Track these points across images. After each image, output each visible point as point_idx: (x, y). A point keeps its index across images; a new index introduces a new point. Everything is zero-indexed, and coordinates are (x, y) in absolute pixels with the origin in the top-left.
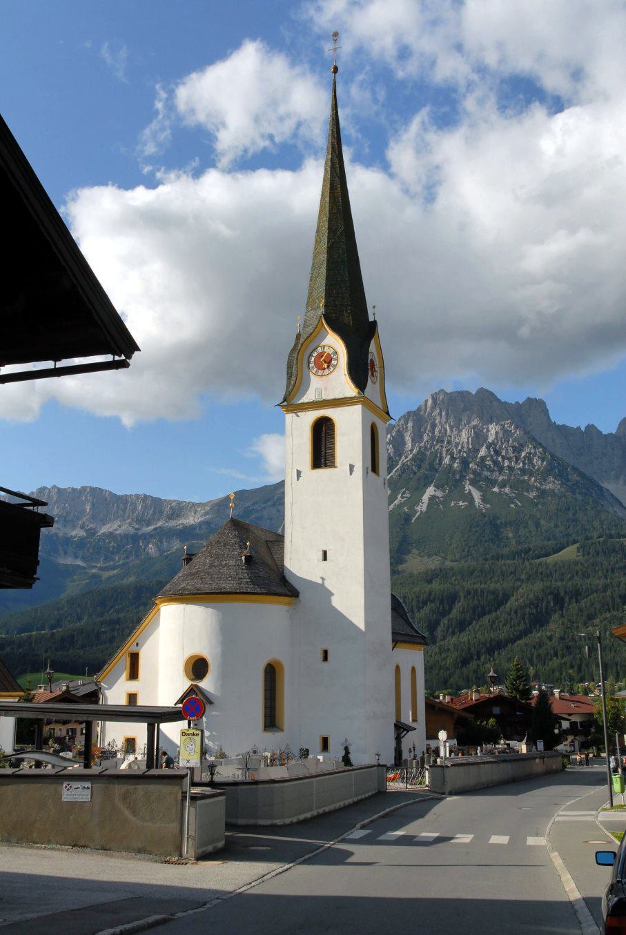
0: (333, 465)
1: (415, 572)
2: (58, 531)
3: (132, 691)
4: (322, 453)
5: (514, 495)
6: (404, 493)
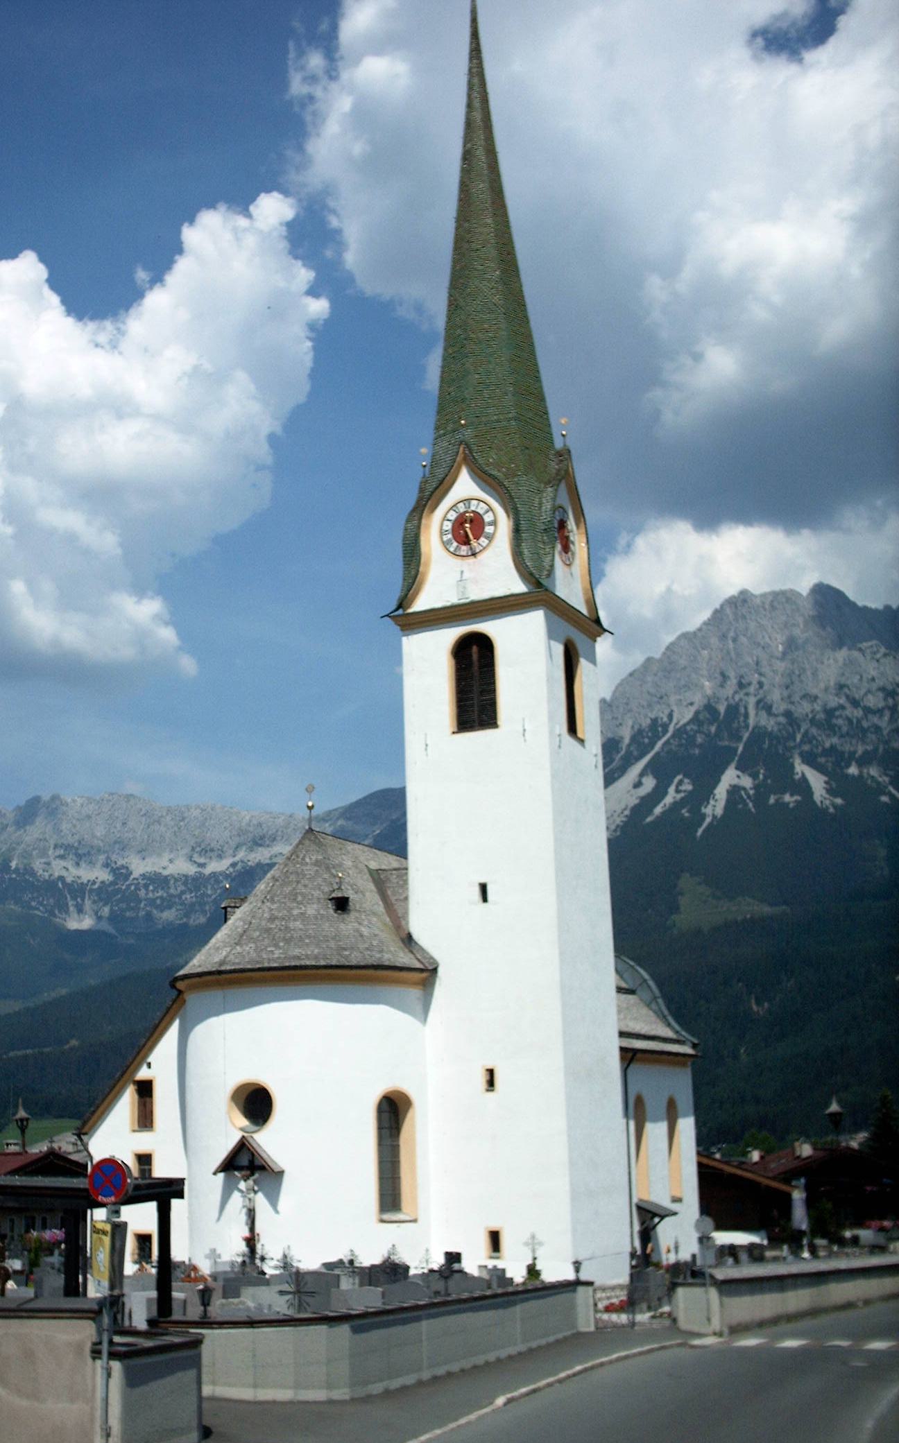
2: (64, 873)
3: (143, 1149)
4: (475, 703)
6: (680, 782)
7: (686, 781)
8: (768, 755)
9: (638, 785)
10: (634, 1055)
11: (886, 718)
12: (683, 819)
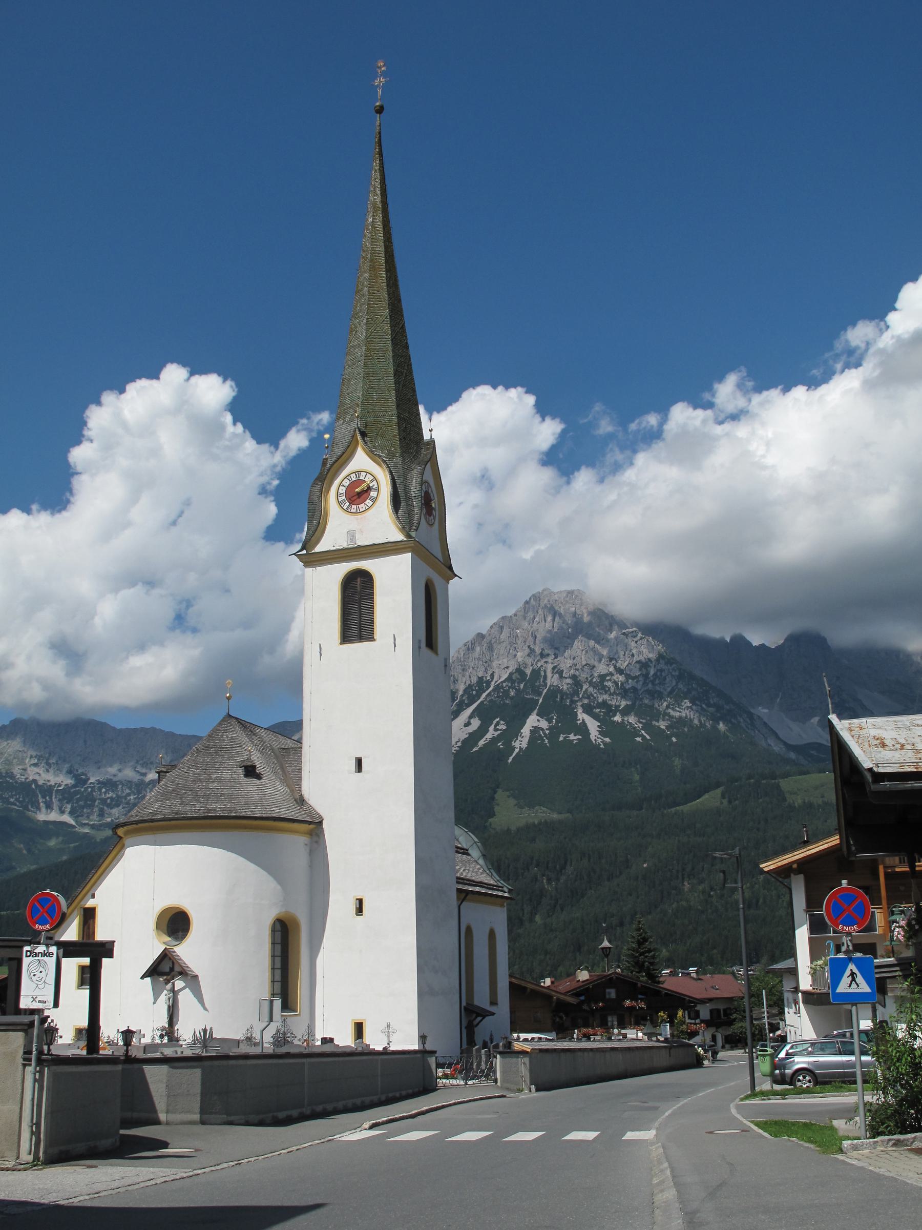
0: (372, 639)
1: (513, 828)
2: (37, 777)
4: (356, 620)
5: (640, 725)
6: (498, 723)
7: (502, 722)
8: (559, 706)
9: (467, 724)
10: (466, 896)
11: (641, 683)
12: (499, 750)
